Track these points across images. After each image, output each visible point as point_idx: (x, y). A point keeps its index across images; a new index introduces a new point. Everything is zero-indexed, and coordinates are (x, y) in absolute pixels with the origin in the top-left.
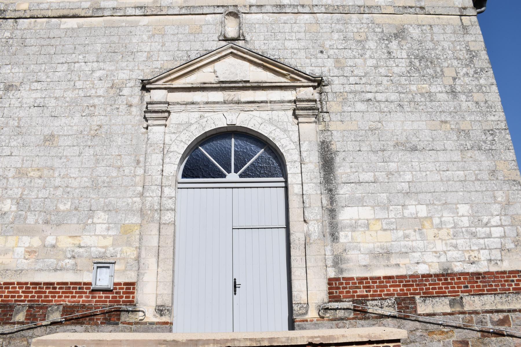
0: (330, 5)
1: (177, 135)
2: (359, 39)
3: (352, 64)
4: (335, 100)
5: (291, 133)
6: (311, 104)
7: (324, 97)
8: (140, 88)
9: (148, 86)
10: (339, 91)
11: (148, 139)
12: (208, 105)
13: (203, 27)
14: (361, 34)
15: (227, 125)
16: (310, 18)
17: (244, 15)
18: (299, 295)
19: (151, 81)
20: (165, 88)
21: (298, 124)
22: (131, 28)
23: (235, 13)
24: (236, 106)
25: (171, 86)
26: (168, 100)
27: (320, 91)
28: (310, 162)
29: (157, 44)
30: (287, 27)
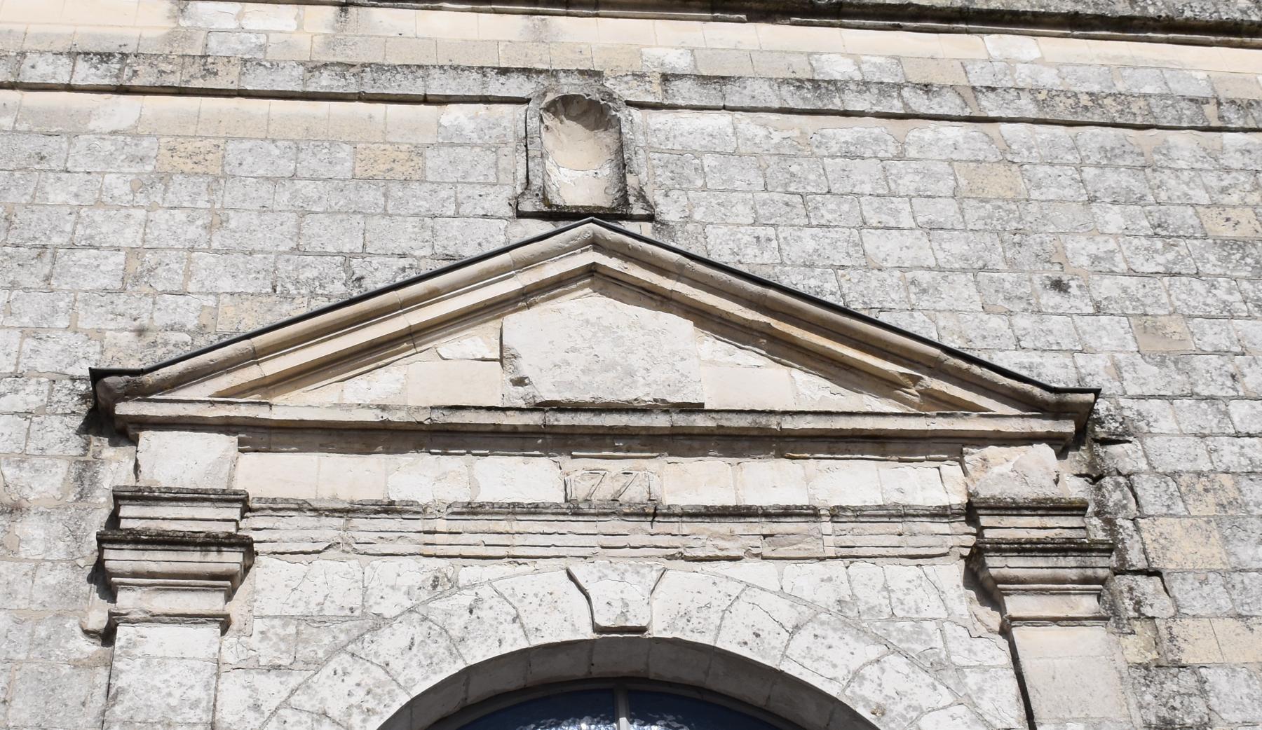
0: (1052, 94)
1: (295, 680)
2: (1228, 232)
3: (1224, 344)
4: (1179, 508)
5: (972, 679)
6: (1058, 527)
7: (1117, 496)
8: (78, 422)
9: (125, 409)
10: (1189, 466)
11: (111, 695)
12: (480, 524)
13: (428, 153)
14: (1232, 214)
15: (598, 629)
16: (967, 139)
17: (637, 114)
19: (149, 379)
20: (226, 426)
21: (1005, 632)
22: (43, 140)
23: (593, 103)
24: (639, 532)
25: (263, 413)
26: (238, 486)
27: (1092, 465)
29: (180, 215)
30: (864, 176)
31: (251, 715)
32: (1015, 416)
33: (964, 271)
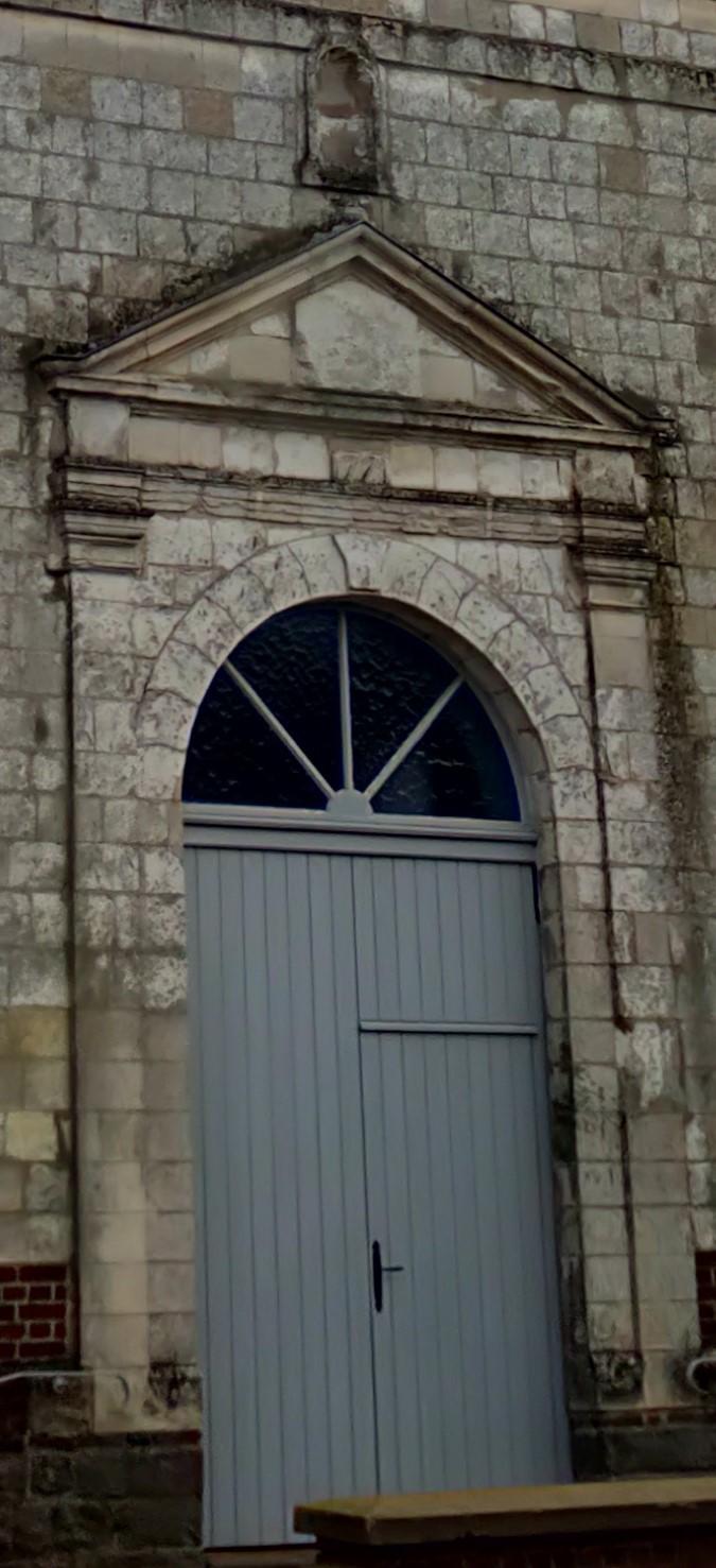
5: (562, 645)
18: (608, 1323)
28: (633, 779)
31: (152, 645)
32: (618, 432)
33: (594, 268)
